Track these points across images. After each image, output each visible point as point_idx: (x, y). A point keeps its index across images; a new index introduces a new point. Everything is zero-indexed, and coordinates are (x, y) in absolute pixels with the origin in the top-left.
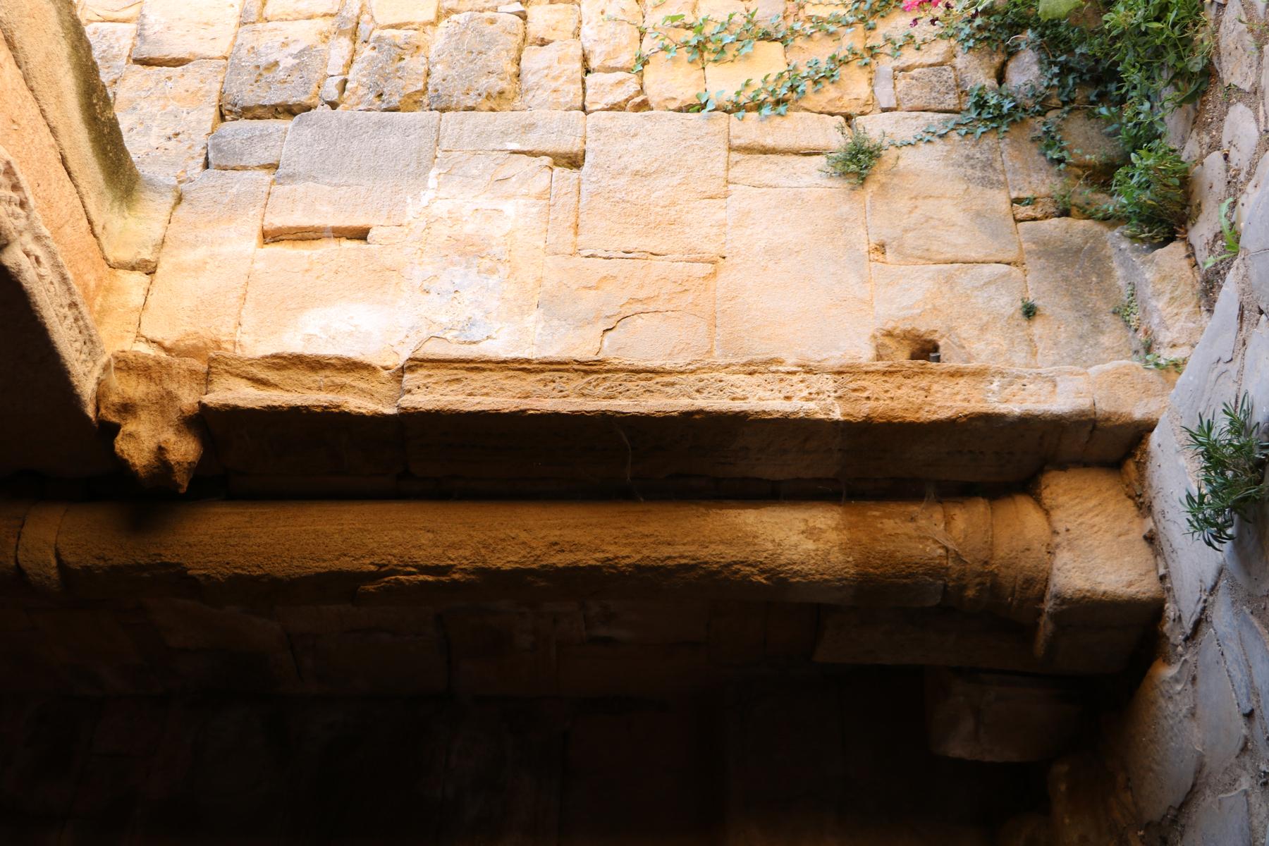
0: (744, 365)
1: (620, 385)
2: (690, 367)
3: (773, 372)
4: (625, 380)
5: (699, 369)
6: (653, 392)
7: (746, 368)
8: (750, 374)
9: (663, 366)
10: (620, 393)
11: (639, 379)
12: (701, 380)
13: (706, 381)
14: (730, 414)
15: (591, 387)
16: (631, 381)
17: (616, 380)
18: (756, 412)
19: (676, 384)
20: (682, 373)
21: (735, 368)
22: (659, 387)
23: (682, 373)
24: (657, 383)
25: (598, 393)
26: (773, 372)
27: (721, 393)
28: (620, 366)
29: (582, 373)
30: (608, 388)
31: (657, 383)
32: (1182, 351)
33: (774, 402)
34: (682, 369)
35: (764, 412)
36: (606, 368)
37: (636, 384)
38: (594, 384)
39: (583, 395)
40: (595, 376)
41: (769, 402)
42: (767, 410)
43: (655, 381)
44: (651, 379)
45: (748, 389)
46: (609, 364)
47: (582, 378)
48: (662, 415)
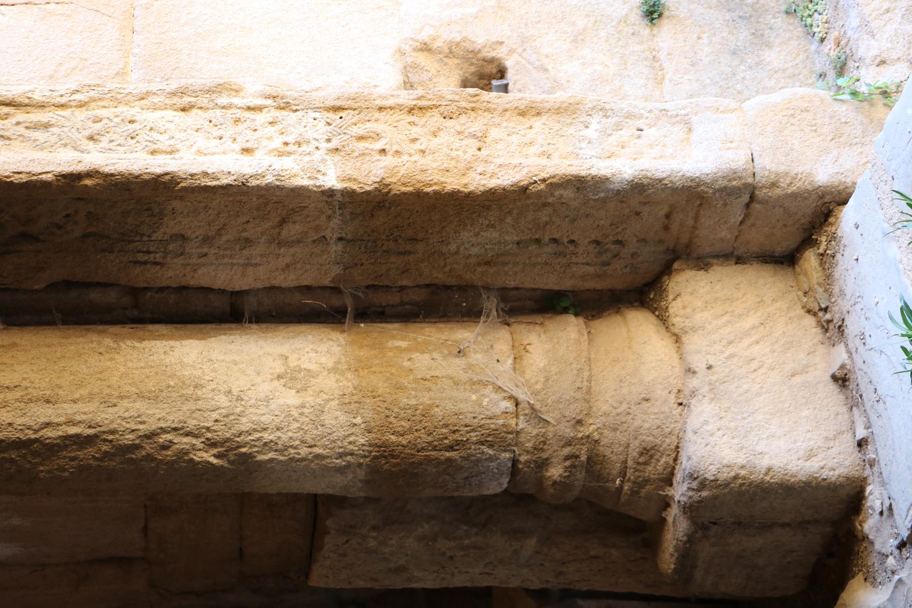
0: (173, 94)
2: (78, 97)
3: (223, 108)
6: (9, 139)
7: (176, 100)
9: (30, 95)
12: (98, 120)
18: (192, 175)
20: (62, 106)
21: (156, 100)
22: (21, 130)
23: (62, 106)
24: (18, 123)
26: (223, 108)
27: (133, 141)
34: (63, 100)
42: (210, 171)
43: (13, 120)
45: (179, 135)
48: (24, 178)
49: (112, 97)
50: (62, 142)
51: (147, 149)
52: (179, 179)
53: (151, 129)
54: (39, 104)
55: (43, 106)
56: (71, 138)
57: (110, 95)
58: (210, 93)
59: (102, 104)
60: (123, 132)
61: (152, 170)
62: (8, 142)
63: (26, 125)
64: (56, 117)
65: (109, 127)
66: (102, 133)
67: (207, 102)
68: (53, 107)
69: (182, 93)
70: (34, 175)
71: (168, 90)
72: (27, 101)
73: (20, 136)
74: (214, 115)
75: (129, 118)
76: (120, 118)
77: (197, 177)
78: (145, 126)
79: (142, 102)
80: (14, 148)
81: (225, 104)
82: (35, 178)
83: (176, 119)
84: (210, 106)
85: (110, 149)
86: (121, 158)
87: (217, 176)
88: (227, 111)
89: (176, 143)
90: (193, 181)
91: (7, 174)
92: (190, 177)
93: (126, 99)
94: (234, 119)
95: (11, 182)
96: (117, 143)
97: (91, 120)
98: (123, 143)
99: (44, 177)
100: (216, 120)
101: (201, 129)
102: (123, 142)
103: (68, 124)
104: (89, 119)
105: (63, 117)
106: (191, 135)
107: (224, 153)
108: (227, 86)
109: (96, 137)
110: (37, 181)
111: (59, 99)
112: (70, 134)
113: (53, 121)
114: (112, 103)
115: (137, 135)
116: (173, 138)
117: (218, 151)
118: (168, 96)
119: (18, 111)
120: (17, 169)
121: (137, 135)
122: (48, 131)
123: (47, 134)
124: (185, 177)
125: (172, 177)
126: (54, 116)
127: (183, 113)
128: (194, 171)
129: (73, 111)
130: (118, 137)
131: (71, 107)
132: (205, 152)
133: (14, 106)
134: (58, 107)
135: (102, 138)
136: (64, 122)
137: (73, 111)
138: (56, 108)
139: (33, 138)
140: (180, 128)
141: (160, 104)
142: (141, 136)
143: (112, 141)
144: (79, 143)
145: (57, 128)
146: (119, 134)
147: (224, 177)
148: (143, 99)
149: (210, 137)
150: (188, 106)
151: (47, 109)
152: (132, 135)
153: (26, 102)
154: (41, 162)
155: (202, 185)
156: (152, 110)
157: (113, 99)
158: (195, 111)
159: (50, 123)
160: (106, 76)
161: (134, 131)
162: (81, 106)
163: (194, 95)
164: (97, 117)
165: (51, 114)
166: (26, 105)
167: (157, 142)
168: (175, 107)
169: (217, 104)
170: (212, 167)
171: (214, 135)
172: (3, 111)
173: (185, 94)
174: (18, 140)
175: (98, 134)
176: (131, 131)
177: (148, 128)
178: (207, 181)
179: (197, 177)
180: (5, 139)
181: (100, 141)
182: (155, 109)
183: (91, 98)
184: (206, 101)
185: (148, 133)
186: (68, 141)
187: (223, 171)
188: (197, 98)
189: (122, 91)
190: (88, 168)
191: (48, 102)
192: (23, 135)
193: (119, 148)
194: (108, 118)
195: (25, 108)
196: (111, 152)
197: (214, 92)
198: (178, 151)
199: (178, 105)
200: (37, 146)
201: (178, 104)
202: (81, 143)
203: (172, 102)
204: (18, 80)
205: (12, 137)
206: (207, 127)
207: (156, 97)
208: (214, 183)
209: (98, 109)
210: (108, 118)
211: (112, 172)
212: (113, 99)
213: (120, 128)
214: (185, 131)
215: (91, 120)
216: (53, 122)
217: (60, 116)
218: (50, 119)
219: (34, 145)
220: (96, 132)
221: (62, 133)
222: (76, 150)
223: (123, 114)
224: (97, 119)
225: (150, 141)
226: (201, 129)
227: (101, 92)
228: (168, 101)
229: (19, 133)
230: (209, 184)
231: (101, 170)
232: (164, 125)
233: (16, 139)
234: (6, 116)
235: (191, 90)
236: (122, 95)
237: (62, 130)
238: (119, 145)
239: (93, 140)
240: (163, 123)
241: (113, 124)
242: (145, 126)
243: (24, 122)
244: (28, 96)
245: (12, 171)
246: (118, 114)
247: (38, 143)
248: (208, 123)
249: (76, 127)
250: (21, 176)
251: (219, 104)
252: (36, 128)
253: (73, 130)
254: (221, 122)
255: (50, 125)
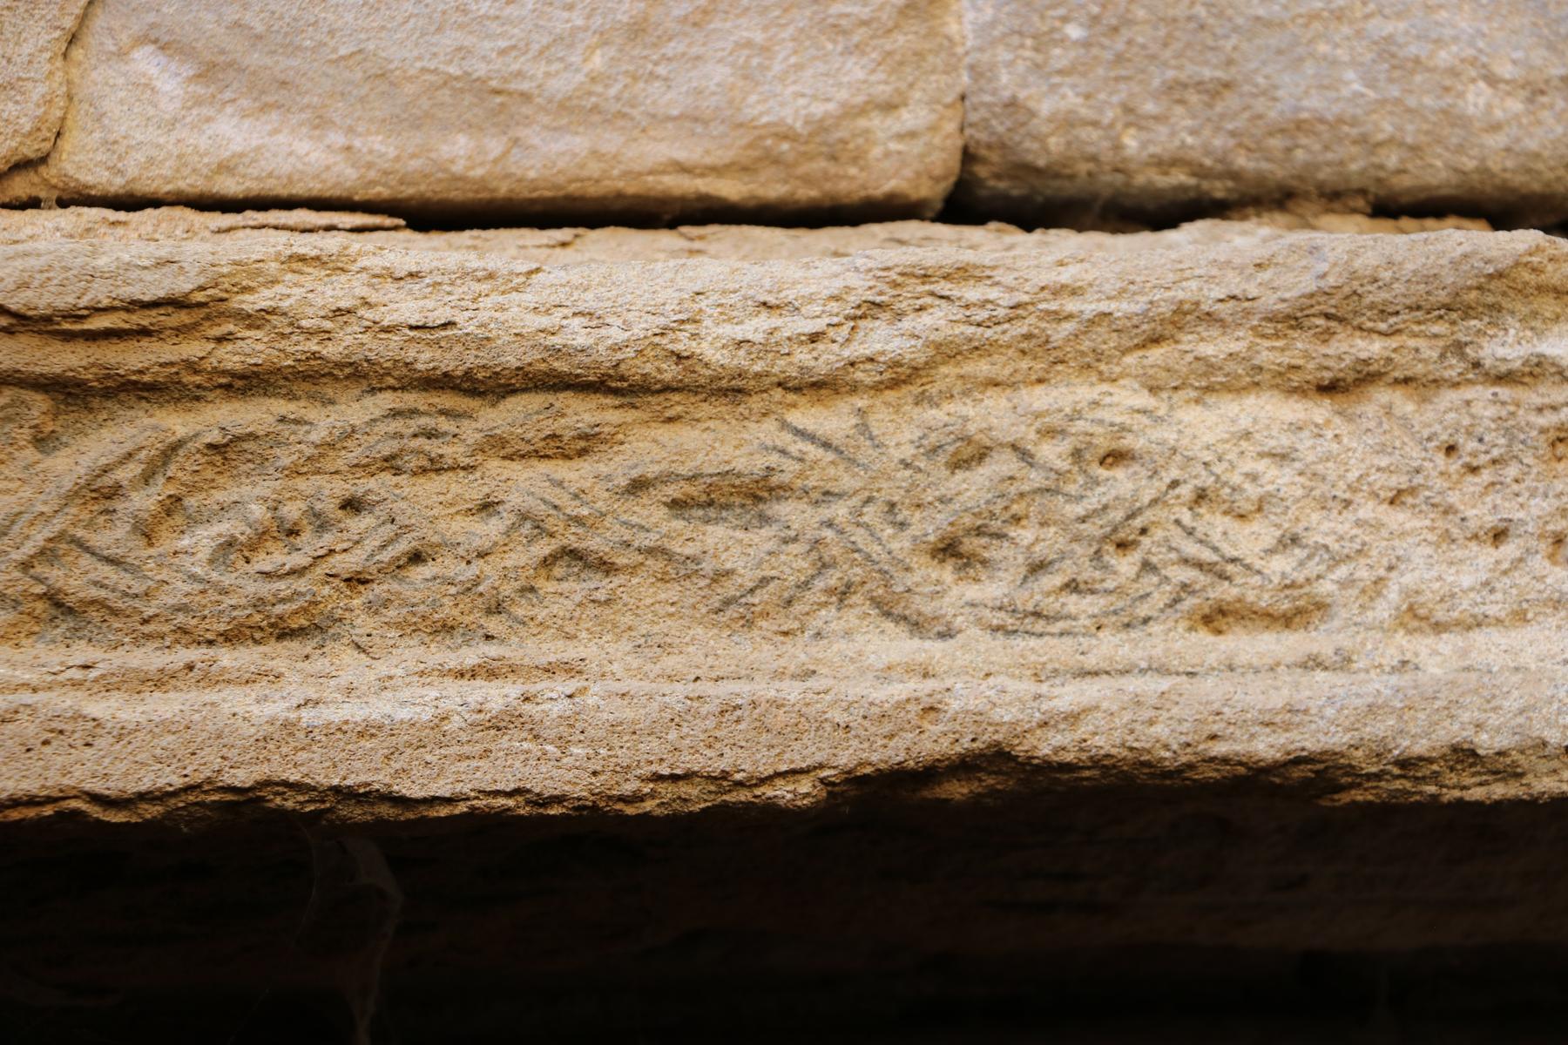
0: (1291, 320)
1: (352, 505)
2: (882, 339)
3: (1505, 378)
4: (391, 464)
5: (947, 352)
6: (606, 567)
7: (1301, 349)
8: (1330, 389)
9: (683, 345)
10: (357, 581)
11: (496, 444)
12: (971, 455)
13: (1002, 464)
14: (1211, 774)
15: (107, 538)
16: (435, 467)
17: (312, 464)
18: (1405, 764)
19: (780, 492)
20: (820, 387)
21: (1215, 346)
22: (650, 513)
23: (820, 387)
24: (638, 486)
25: (180, 589)
26: (1505, 378)
27: (1126, 565)
28: (344, 343)
29: (39, 404)
30: (260, 538)
31: (638, 486)
32: (1091, 604)
33: (1518, 637)
34: (824, 360)
35: (1464, 756)
36: (231, 358)
37: (471, 489)
38: (144, 501)
39: (59, 605)
40: (176, 423)
41: (1490, 646)
42: (1486, 743)
43: (617, 466)
44: (587, 444)
45: (1324, 528)
46: (255, 320)
47: (43, 441)
48: (697, 797)
49: (1028, 337)
50: (832, 579)
51: (1189, 602)
52: (1347, 774)
53: (1201, 496)
54: (724, 383)
55: (740, 391)
56: (868, 557)
57: (1020, 328)
58: (1454, 316)
59: (981, 368)
60: (1083, 520)
61: (1238, 748)
62: (603, 586)
63: (673, 491)
64: (798, 446)
65: (1022, 495)
66: (995, 525)
67: (1435, 355)
68: (778, 394)
69: (1328, 316)
70: (740, 784)
71: (1270, 302)
72: (670, 372)
73: (651, 551)
74: (1466, 421)
75: (1104, 444)
76: (1065, 446)
77: (1425, 771)
78: (1174, 484)
79: (1156, 354)
80: (628, 619)
81: (1517, 365)
82: (743, 796)
83: (1305, 443)
84: (1447, 374)
85: (1037, 614)
86: (1091, 662)
87: (1515, 764)
88: (1520, 393)
89: (1313, 568)
90: (1408, 785)
91: (628, 788)
92: (1396, 771)
93: (1086, 345)
94: (1552, 435)
95: (646, 816)
96: (1058, 580)
97: (942, 458)
98: (1085, 576)
99: (782, 792)
100: (1472, 445)
101: (1413, 491)
102: (1088, 573)
103: (847, 482)
104: (935, 450)
105: (826, 445)
106: (1377, 526)
107: (1520, 617)
108: (1527, 276)
109: (970, 544)
110: (748, 806)
111: (803, 356)
112: (860, 536)
113: (788, 471)
114: (1024, 364)
115: (1144, 531)
116: (1295, 540)
117: (1492, 610)
118: (1269, 329)
119: (631, 415)
120: (670, 759)
121: (1144, 531)
122: (764, 520)
123: (763, 538)
124: (1374, 769)
125: (1317, 772)
126: (786, 438)
127: (1320, 410)
128: (1420, 748)
129: (861, 412)
130: (1061, 543)
131: (854, 388)
132: (1440, 615)
133: (616, 392)
134: (797, 390)
135: (996, 552)
136: (832, 471)
137: (861, 412)
138: (791, 397)
139: (708, 566)
140: (1321, 489)
141: (1231, 366)
142: (1158, 534)
143: (1038, 568)
144: (901, 582)
145: (802, 505)
146: (1064, 526)
147: (1544, 766)
148: (1156, 340)
149: (1455, 532)
150: (1351, 376)
151: (756, 403)
152: (1122, 535)
153: (667, 377)
154: (769, 720)
155: (1445, 799)
156: (1193, 394)
157: (1036, 344)
158: (1382, 395)
159: (775, 480)
160: (865, 23)
161: (1131, 516)
162: (895, 384)
163: (1383, 326)
164: (968, 440)
165: (767, 431)
166: (667, 389)
167: (1230, 568)
168: (1296, 379)
169: (1477, 365)
170: (1494, 720)
171: (1473, 525)
172: (569, 421)
173: (1341, 320)
174: (642, 572)
175: (979, 531)
176: (1117, 515)
177: (1186, 491)
178: (1468, 781)
179: (1425, 771)
180: (587, 566)
181: (984, 562)
182: (1209, 389)
183: (938, 346)
184: (1430, 352)
185: (1186, 518)
186: (857, 573)
187: (1545, 744)
188: (1393, 342)
189: (1071, 305)
190: (966, 743)
191: (758, 376)
192: (664, 551)
193: (1072, 602)
194: (1014, 447)
195: (661, 398)
196: (1040, 626)
197: (1468, 312)
198: (1321, 606)
199: (1311, 372)
200: (727, 602)
201: (1311, 366)
202: (910, 579)
203: (1286, 359)
204: (503, 52)
205: (621, 561)
206: (1439, 483)
207: (1215, 332)
208: (1499, 791)
209: (966, 393)
210: (1014, 447)
211: (1069, 757)
212: (1036, 344)
213: (1070, 498)
214: (1347, 503)
215: (942, 458)
216: (785, 478)
217: (810, 437)
218: (773, 460)
219: (715, 602)
220: (968, 520)
221: (829, 534)
222: (888, 614)
223: (1080, 425)
224: (968, 452)
225: (1200, 565)
226: (1413, 491)
227: (982, 315)
228: (1269, 355)
229: (650, 540)
230: (1477, 794)
231: (1020, 750)
232: (1253, 477)
233: (633, 569)
234: (582, 444)
235: (1372, 306)
236: (1069, 327)
237: (825, 513)
238: (1072, 586)
239: (959, 555)
240: (1248, 466)
241: (1036, 479)
242: (1174, 484)
243: (667, 478)
244: (678, 347)
245: (646, 770)
246: (1056, 420)
247: (729, 589)
248: (1440, 458)
249: (882, 497)
250: (684, 789)
251: (1488, 363)
252: (711, 504)
253: (871, 514)
254: (1495, 453)
255: (771, 490)
